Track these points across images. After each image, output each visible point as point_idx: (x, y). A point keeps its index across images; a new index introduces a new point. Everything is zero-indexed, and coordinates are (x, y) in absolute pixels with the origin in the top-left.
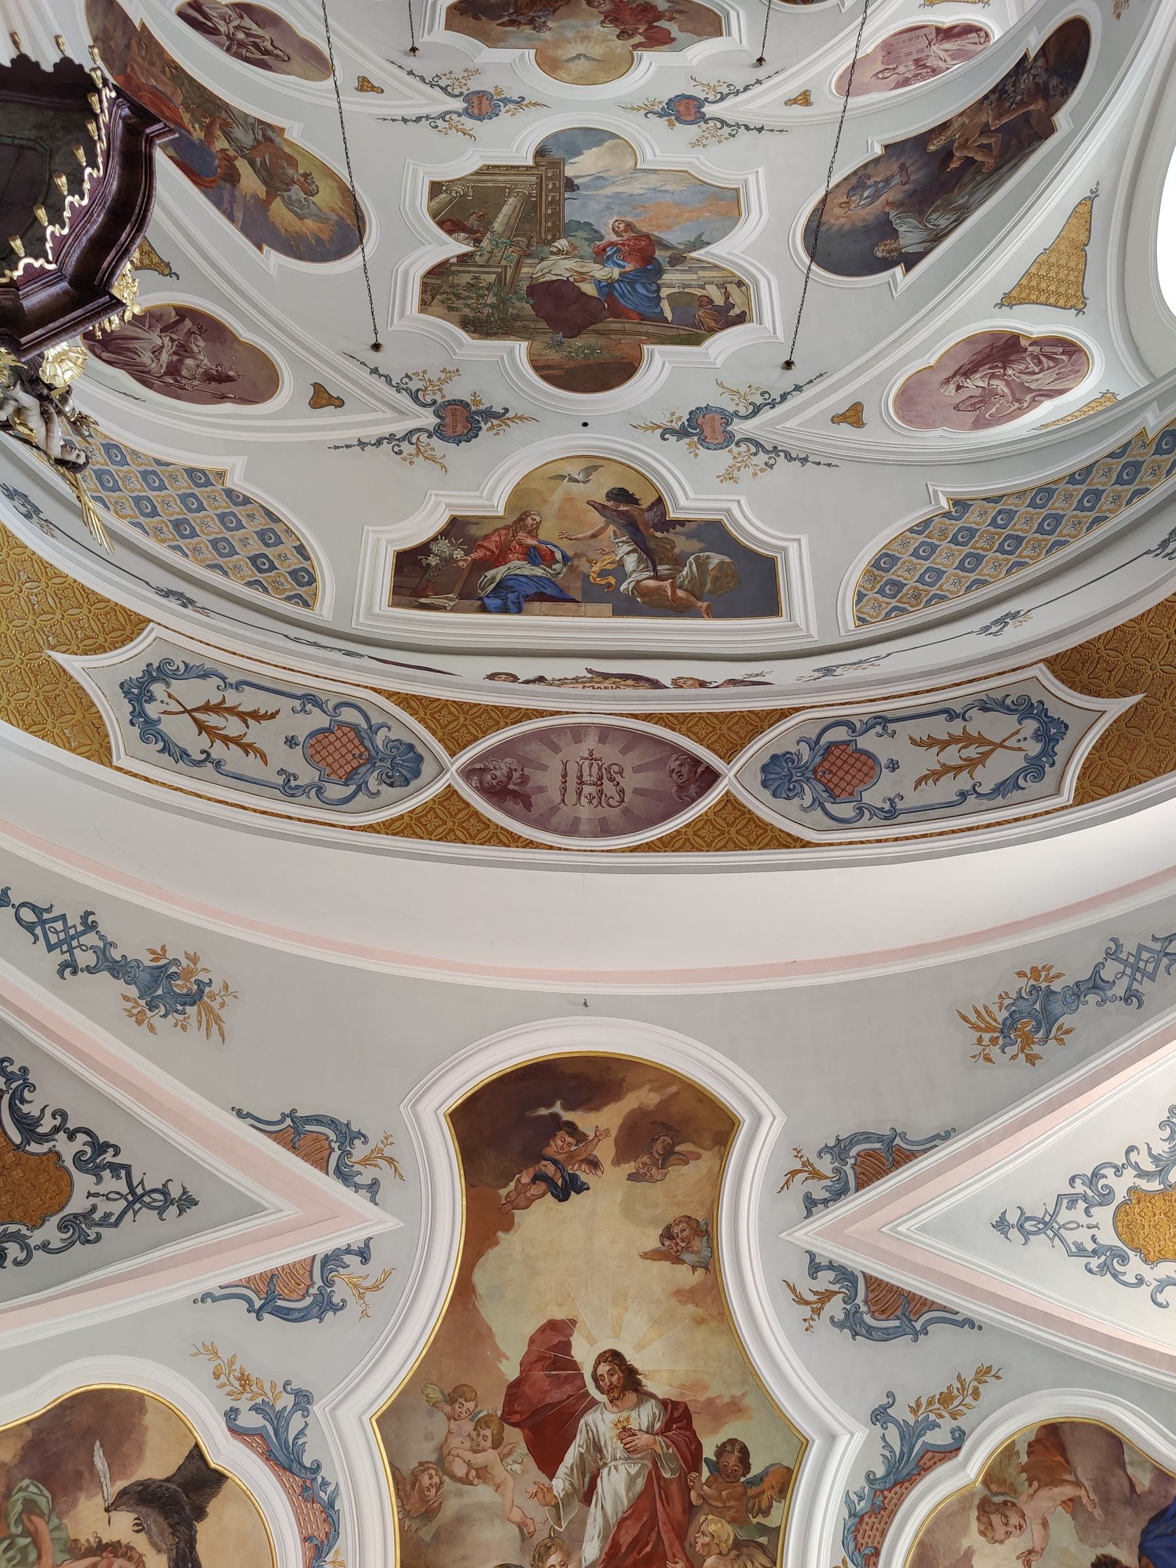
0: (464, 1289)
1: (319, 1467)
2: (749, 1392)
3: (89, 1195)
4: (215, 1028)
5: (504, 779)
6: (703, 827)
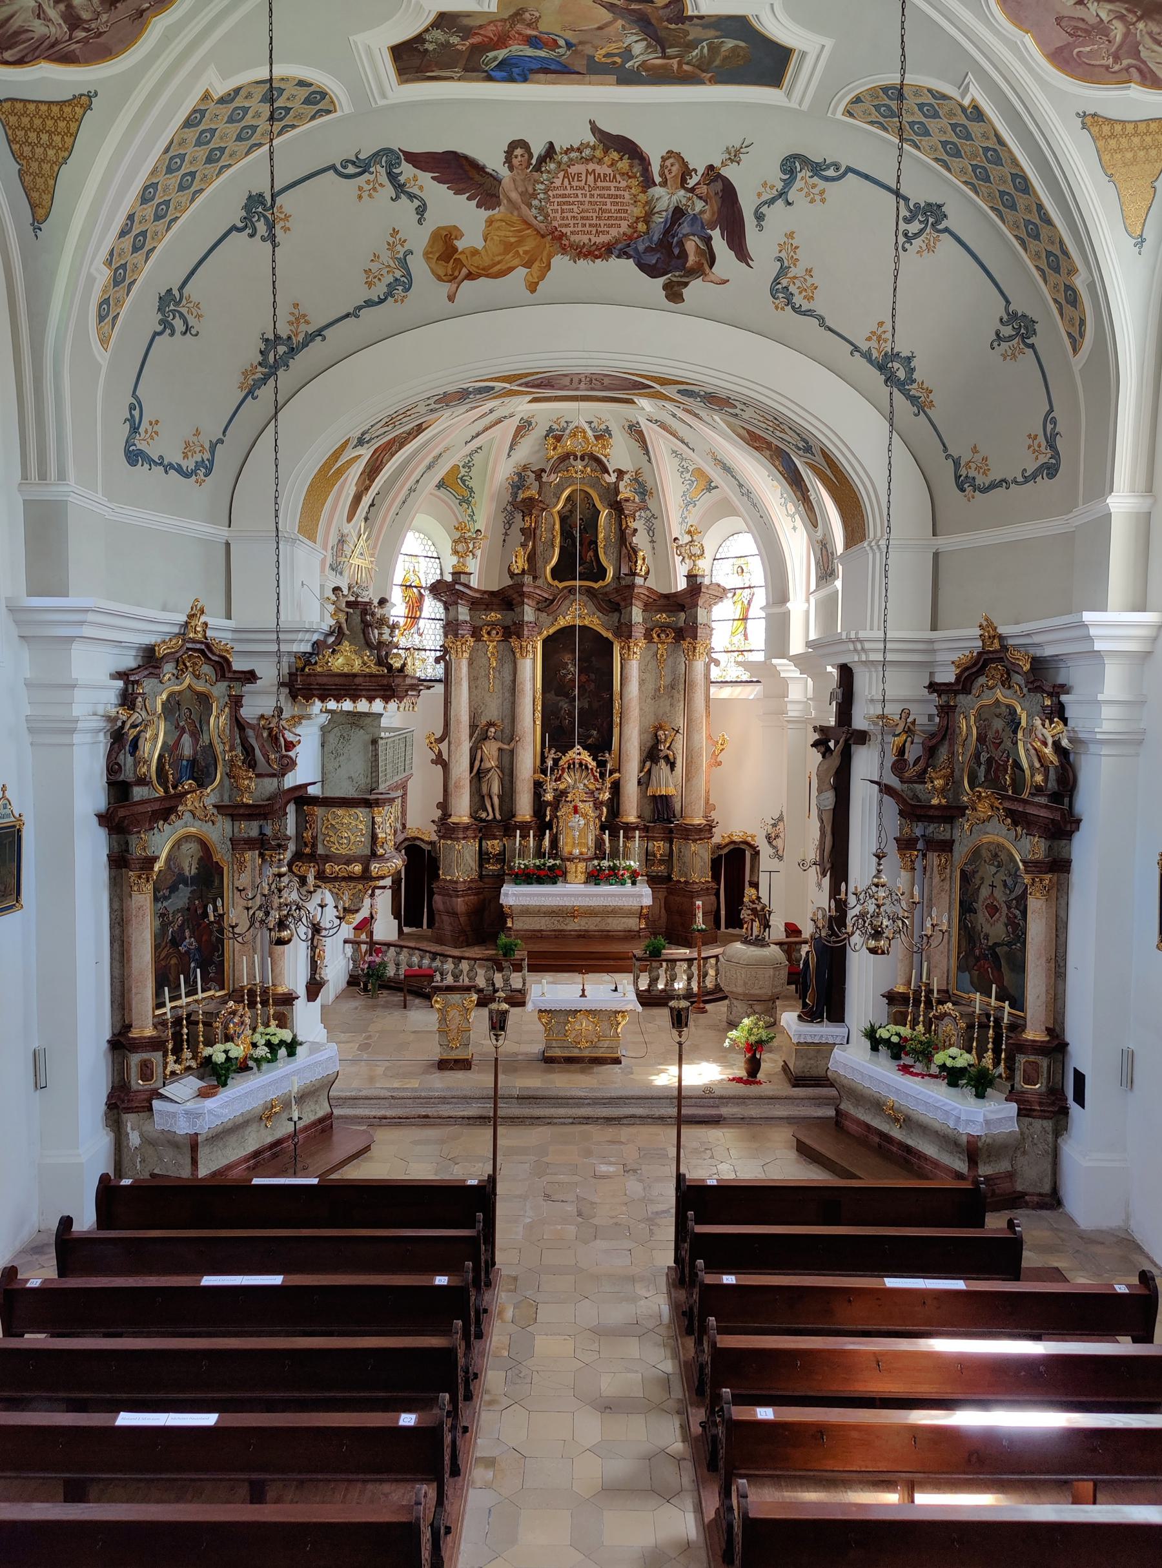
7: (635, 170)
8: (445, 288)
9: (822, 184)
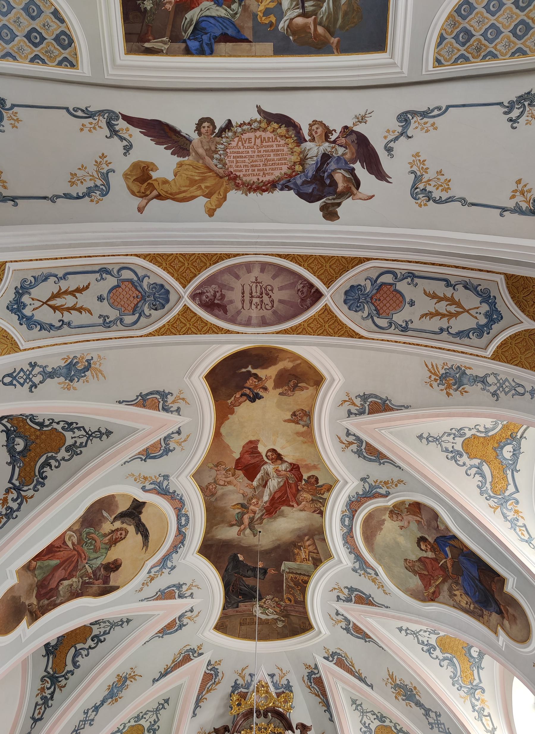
0: (218, 434)
1: (175, 491)
2: (319, 463)
3: (72, 438)
4: (391, 674)
5: (212, 298)
6: (312, 322)
7: (290, 133)
8: (137, 201)
9: (431, 121)
